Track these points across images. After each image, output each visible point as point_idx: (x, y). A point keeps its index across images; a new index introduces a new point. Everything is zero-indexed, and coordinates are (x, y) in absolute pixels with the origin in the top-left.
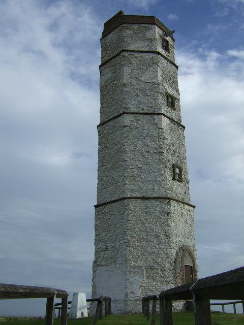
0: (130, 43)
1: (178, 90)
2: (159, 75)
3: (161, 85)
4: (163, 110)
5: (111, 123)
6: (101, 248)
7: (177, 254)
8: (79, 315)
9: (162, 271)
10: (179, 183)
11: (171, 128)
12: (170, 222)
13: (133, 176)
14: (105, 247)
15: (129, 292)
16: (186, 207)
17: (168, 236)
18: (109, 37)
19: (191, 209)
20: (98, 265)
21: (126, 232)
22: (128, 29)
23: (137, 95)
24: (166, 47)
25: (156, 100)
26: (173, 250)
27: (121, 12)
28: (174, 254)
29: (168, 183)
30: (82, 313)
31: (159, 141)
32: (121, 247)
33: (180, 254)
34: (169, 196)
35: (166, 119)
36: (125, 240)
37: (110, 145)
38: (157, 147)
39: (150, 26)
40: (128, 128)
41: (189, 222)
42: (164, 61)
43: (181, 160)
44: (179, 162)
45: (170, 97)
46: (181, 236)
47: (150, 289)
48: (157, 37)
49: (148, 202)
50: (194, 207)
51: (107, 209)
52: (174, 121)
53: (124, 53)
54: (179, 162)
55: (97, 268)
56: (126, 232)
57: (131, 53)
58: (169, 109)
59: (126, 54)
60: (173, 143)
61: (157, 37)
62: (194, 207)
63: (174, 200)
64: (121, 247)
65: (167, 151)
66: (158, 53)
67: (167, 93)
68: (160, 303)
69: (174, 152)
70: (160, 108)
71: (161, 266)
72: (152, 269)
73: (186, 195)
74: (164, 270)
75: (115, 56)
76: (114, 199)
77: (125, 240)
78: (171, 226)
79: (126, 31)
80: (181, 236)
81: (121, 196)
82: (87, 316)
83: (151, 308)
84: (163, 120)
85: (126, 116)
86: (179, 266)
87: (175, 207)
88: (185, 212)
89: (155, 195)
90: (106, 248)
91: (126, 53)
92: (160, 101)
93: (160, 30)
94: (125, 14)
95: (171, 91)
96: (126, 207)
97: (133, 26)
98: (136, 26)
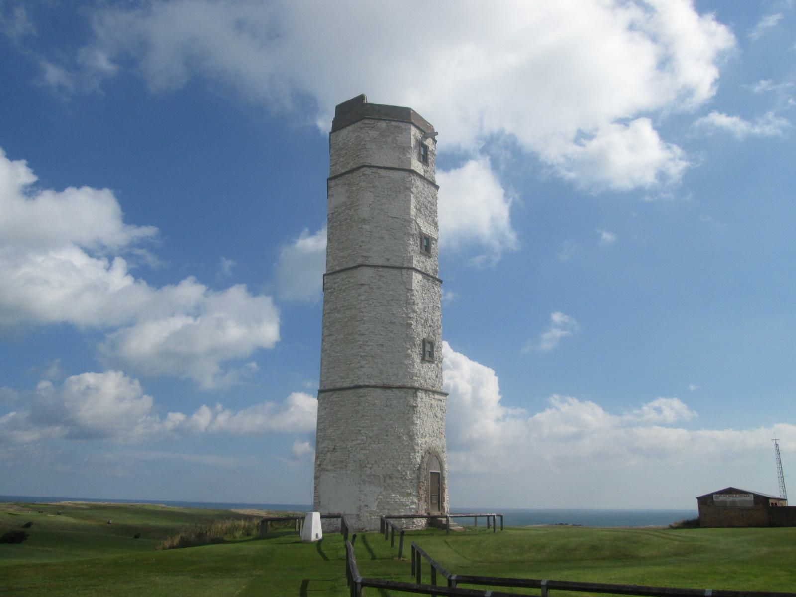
0: (374, 153)
1: (436, 225)
2: (412, 207)
3: (414, 222)
4: (415, 262)
5: (343, 275)
6: (327, 447)
7: (423, 457)
8: (313, 538)
9: (403, 480)
10: (429, 365)
11: (423, 286)
12: (415, 419)
13: (372, 356)
14: (333, 447)
15: (363, 505)
16: (437, 396)
17: (412, 437)
18: (344, 133)
19: (442, 398)
20: (323, 469)
21: (360, 431)
22: (372, 128)
23: (382, 238)
24: (423, 156)
25: (406, 245)
26: (417, 454)
27: (361, 98)
28: (419, 460)
29: (416, 366)
30: (317, 535)
31: (407, 308)
32: (354, 449)
33: (426, 460)
34: (417, 385)
35: (417, 274)
36: (359, 442)
37: (341, 307)
38: (404, 316)
39: (403, 125)
40: (368, 286)
41: (439, 416)
42: (419, 183)
43: (434, 331)
44: (431, 334)
45: (426, 238)
46: (428, 435)
47: (388, 502)
48: (413, 143)
49: (389, 391)
50: (446, 394)
51: (336, 396)
52: (428, 275)
53: (364, 169)
54: (431, 334)
55: (322, 472)
56: (360, 431)
57: (374, 170)
58: (423, 258)
59: (368, 171)
60: (425, 308)
61: (413, 143)
62: (446, 394)
63: (422, 389)
64: (354, 449)
65: (417, 322)
66: (413, 172)
67: (421, 232)
68: (261, 355)
69: (426, 321)
70: (411, 259)
71: (402, 474)
72: (390, 477)
73: (438, 379)
74: (406, 479)
75: (351, 171)
76: (345, 385)
77: (359, 442)
78: (417, 424)
79: (369, 132)
80: (428, 435)
81: (356, 383)
82: (446, 585)
83: (385, 527)
84: (414, 277)
85: (364, 269)
86: (424, 473)
87: (422, 398)
88: (434, 403)
89: (399, 384)
90: (334, 449)
91: (368, 169)
92: (410, 248)
93: (418, 131)
94: (368, 102)
95: (427, 229)
96: (361, 399)
97: (379, 124)
98: (383, 125)
